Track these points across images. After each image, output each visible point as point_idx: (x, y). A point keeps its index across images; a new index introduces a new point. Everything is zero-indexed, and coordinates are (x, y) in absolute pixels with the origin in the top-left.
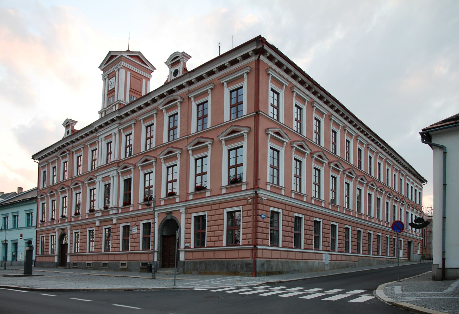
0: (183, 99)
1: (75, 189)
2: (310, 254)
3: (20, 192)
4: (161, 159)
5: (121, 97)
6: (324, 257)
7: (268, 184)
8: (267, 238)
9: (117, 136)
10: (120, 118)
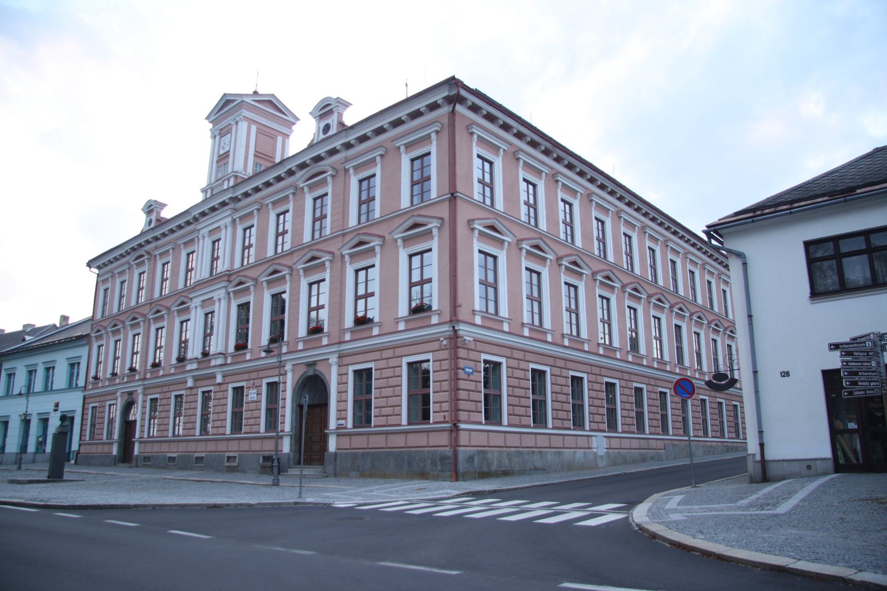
0: (337, 171)
1: (156, 320)
2: (566, 437)
3: (65, 324)
4: (298, 270)
5: (239, 166)
6: (594, 443)
7: (476, 313)
8: (479, 410)
9: (229, 229)
10: (236, 199)
